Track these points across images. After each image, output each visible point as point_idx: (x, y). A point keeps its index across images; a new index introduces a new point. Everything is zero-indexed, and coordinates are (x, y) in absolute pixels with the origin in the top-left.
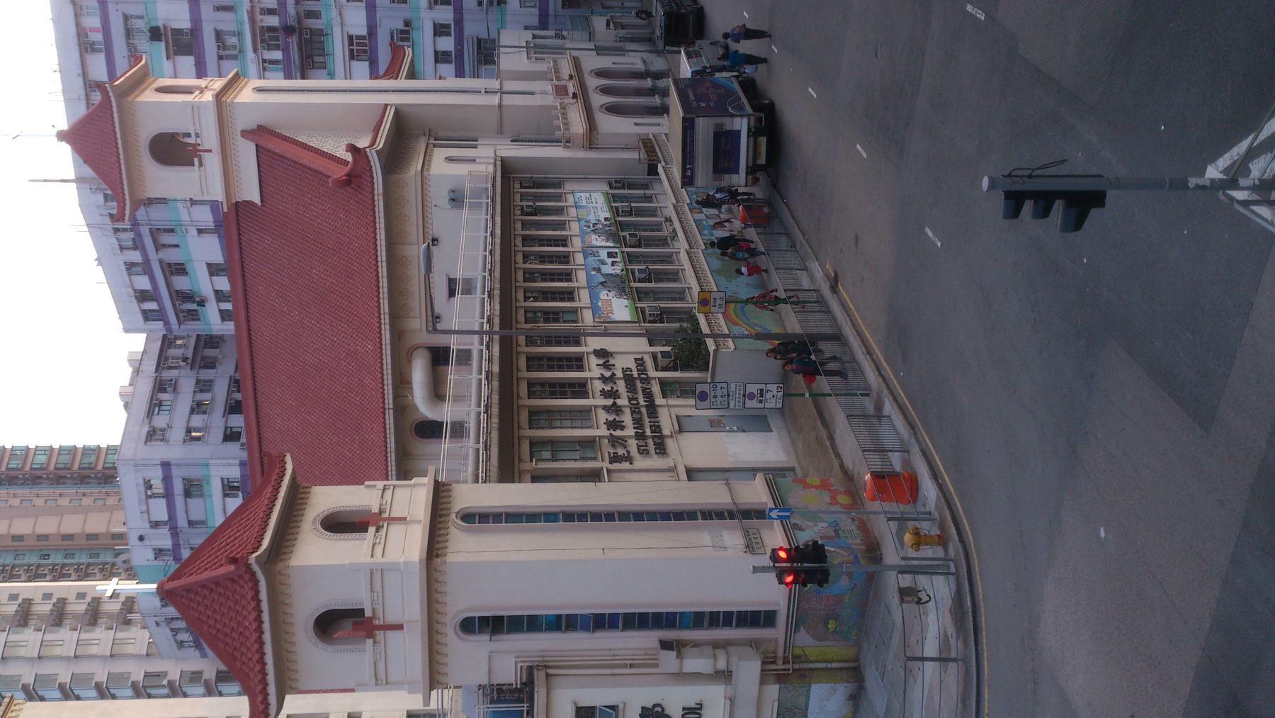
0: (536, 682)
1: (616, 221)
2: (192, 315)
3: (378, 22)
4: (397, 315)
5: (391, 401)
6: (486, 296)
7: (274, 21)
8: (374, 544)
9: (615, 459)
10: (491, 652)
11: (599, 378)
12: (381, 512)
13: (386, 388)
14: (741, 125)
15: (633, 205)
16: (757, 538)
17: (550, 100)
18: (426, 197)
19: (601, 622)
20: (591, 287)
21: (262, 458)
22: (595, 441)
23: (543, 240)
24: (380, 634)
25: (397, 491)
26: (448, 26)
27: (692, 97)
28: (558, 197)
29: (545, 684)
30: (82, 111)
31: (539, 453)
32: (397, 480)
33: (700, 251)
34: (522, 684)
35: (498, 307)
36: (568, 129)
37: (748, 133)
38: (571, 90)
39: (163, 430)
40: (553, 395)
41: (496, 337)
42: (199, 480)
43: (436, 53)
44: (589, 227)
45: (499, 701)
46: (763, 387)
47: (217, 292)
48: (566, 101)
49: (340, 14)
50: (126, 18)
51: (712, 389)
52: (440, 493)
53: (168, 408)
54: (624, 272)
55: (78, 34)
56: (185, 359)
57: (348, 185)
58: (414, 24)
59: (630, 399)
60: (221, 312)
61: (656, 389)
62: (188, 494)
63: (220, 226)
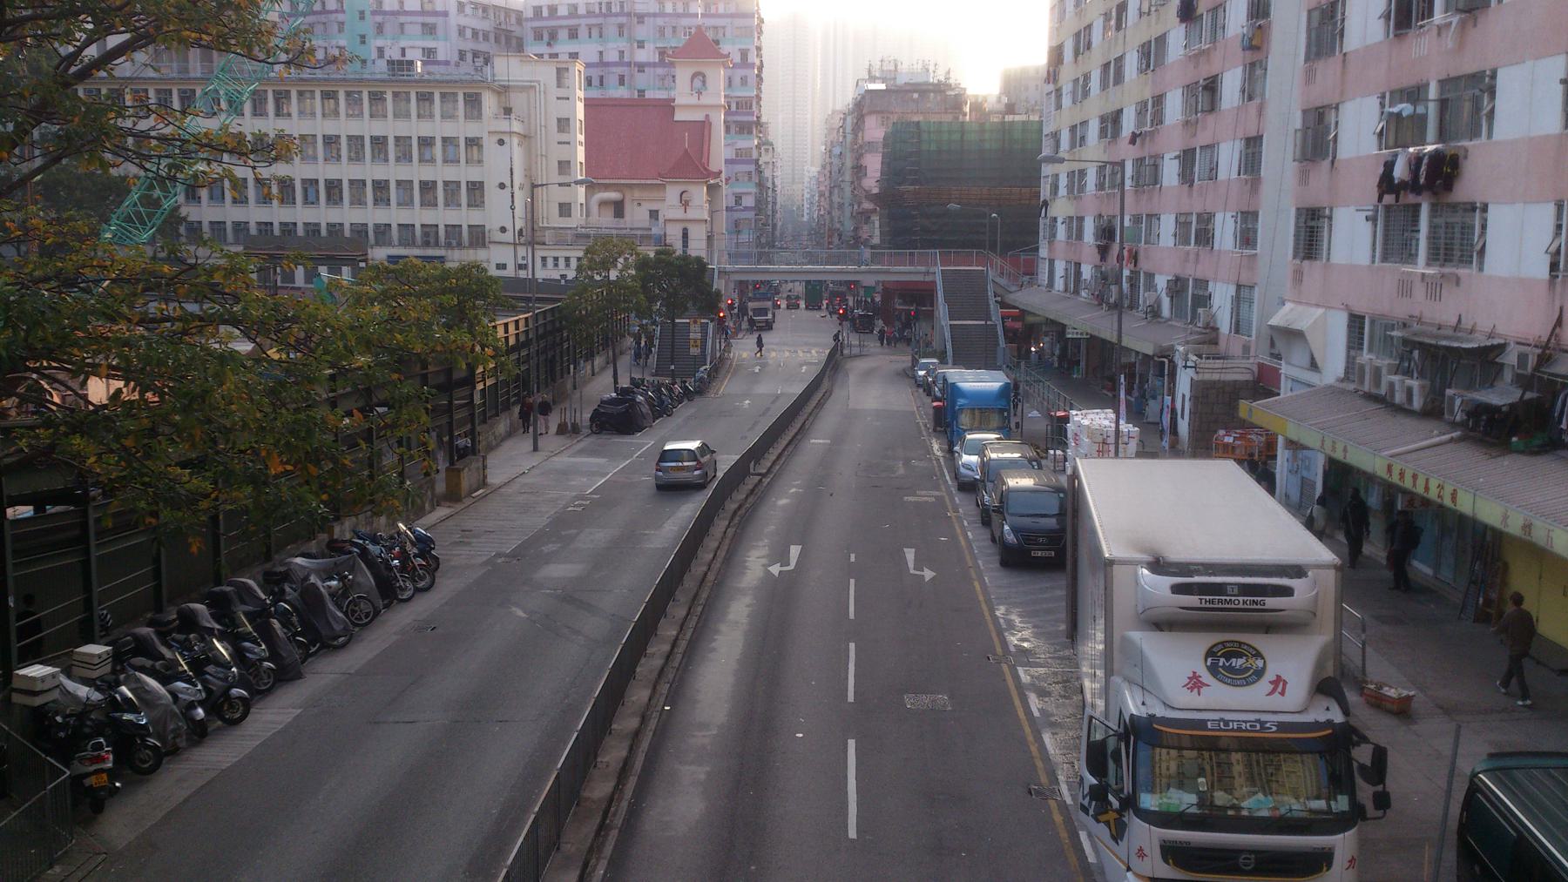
50: (724, 27)
62: (424, 25)
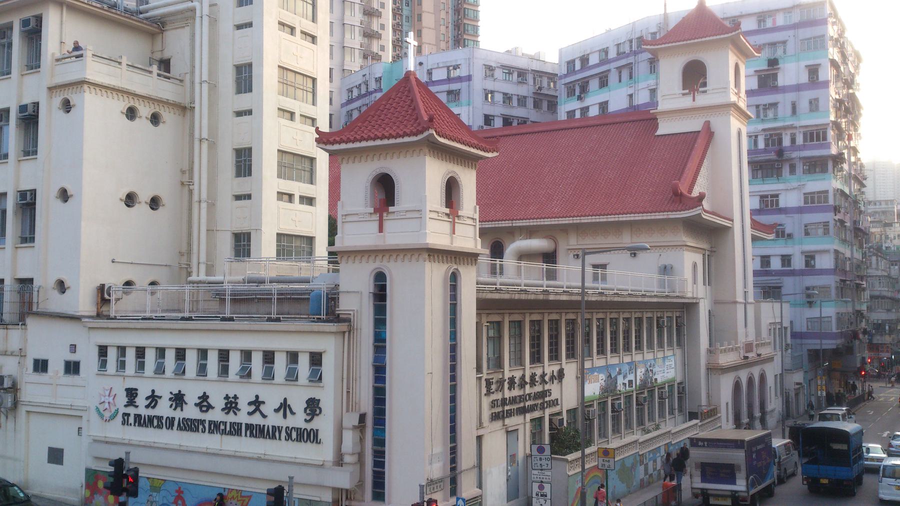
0: (340, 324)
1: (655, 387)
2: (571, 92)
3: (791, 215)
4: (579, 229)
5: (518, 225)
6: (616, 291)
7: (786, 142)
8: (438, 212)
9: (489, 383)
10: (361, 293)
11: (544, 372)
12: (458, 217)
13: (528, 221)
14: (740, 485)
15: (667, 400)
16: (437, 488)
17: (742, 339)
18: (667, 248)
19: (380, 371)
20: (607, 367)
21: (496, 137)
22: (501, 368)
23: (639, 332)
24: (376, 217)
25: (472, 228)
26: (789, 265)
27: (759, 447)
28: (670, 344)
29: (338, 331)
30: (719, 15)
31: (492, 328)
32: (479, 228)
33: (638, 451)
34: (339, 315)
35: (594, 299)
36: (721, 352)
37: (734, 491)
38: (750, 355)
39: (492, 76)
40: (532, 338)
41: (579, 298)
42: (459, 99)
43: (768, 257)
44: (650, 367)
45: (328, 299)
46: (549, 497)
47: (587, 108)
48: (742, 351)
49: (794, 189)
51: (547, 457)
52: (470, 257)
53: (507, 79)
54: (618, 392)
55: (771, 11)
56: (540, 88)
57: (673, 193)
58: (790, 241)
59: (529, 395)
60: (574, 111)
61: (537, 414)
62: (449, 92)
63: (635, 109)
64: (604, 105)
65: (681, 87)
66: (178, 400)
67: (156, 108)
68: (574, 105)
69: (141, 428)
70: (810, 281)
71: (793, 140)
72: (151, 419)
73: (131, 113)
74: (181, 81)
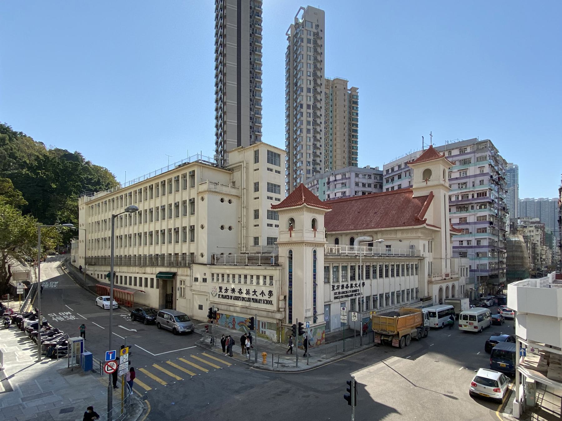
9: (333, 286)
17: (444, 272)
24: (289, 232)
52: (322, 245)
58: (471, 235)
59: (350, 291)
61: (354, 297)
62: (342, 184)
64: (400, 186)
65: (422, 179)
66: (233, 290)
67: (230, 198)
68: (389, 186)
69: (254, 303)
70: (478, 250)
71: (473, 197)
72: (226, 296)
73: (222, 200)
74: (238, 189)
